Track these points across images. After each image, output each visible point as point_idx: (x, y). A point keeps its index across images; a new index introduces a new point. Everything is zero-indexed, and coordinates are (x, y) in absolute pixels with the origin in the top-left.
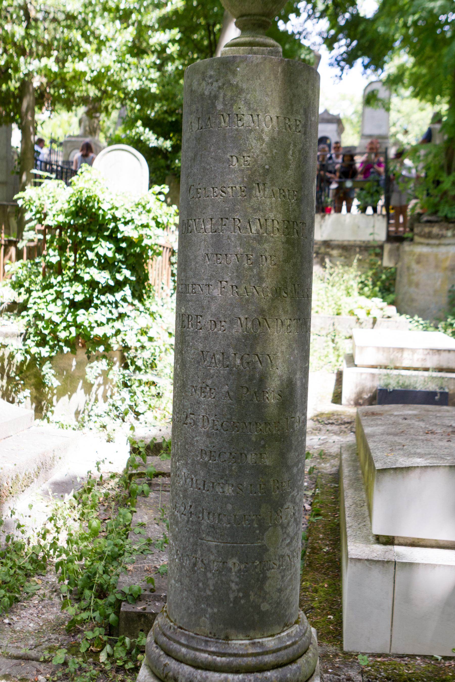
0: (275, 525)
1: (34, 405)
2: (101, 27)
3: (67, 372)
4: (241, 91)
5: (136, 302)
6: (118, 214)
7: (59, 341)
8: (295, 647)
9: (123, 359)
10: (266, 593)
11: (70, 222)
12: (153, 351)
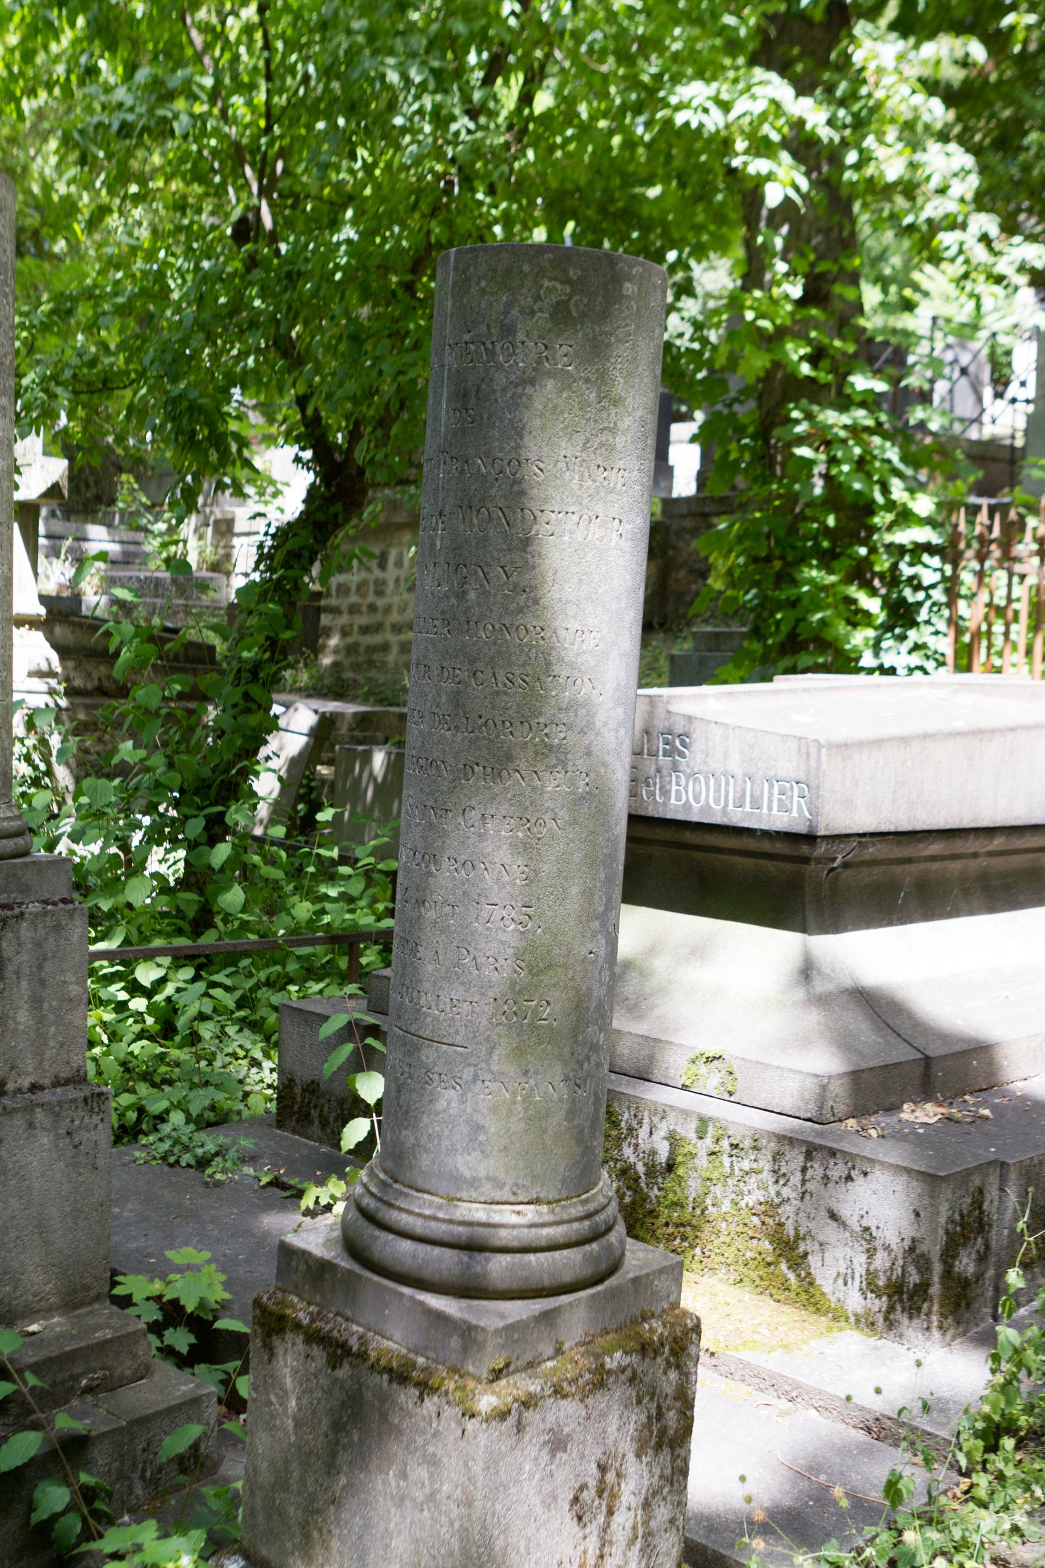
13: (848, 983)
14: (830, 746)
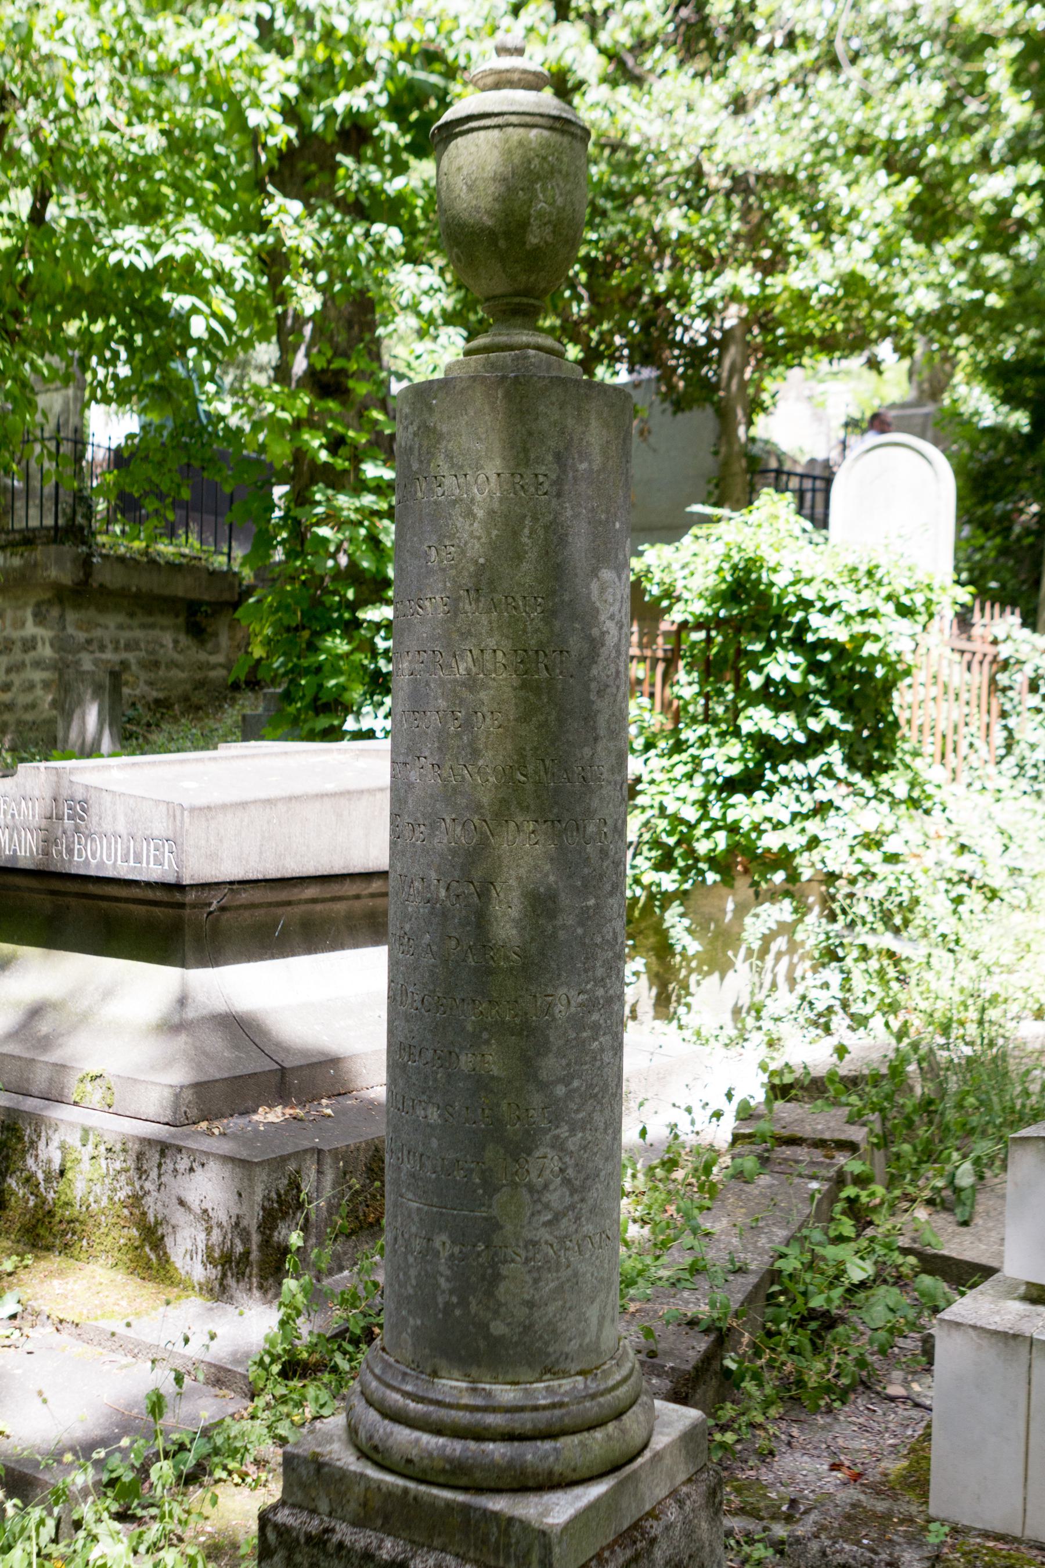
0: (515, 1185)
1: (654, 991)
2: (843, 191)
3: (717, 922)
4: (440, 437)
5: (856, 778)
6: (808, 593)
7: (697, 860)
8: (557, 1412)
9: (828, 899)
10: (500, 1305)
11: (716, 614)
12: (894, 884)
13: (220, 1007)
14: (192, 810)
